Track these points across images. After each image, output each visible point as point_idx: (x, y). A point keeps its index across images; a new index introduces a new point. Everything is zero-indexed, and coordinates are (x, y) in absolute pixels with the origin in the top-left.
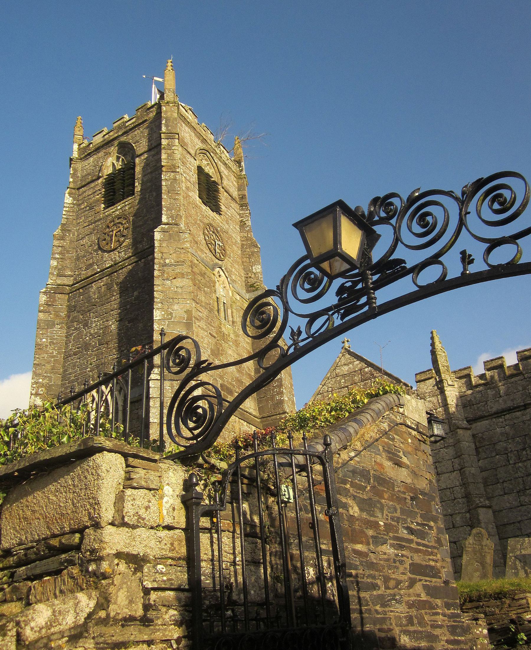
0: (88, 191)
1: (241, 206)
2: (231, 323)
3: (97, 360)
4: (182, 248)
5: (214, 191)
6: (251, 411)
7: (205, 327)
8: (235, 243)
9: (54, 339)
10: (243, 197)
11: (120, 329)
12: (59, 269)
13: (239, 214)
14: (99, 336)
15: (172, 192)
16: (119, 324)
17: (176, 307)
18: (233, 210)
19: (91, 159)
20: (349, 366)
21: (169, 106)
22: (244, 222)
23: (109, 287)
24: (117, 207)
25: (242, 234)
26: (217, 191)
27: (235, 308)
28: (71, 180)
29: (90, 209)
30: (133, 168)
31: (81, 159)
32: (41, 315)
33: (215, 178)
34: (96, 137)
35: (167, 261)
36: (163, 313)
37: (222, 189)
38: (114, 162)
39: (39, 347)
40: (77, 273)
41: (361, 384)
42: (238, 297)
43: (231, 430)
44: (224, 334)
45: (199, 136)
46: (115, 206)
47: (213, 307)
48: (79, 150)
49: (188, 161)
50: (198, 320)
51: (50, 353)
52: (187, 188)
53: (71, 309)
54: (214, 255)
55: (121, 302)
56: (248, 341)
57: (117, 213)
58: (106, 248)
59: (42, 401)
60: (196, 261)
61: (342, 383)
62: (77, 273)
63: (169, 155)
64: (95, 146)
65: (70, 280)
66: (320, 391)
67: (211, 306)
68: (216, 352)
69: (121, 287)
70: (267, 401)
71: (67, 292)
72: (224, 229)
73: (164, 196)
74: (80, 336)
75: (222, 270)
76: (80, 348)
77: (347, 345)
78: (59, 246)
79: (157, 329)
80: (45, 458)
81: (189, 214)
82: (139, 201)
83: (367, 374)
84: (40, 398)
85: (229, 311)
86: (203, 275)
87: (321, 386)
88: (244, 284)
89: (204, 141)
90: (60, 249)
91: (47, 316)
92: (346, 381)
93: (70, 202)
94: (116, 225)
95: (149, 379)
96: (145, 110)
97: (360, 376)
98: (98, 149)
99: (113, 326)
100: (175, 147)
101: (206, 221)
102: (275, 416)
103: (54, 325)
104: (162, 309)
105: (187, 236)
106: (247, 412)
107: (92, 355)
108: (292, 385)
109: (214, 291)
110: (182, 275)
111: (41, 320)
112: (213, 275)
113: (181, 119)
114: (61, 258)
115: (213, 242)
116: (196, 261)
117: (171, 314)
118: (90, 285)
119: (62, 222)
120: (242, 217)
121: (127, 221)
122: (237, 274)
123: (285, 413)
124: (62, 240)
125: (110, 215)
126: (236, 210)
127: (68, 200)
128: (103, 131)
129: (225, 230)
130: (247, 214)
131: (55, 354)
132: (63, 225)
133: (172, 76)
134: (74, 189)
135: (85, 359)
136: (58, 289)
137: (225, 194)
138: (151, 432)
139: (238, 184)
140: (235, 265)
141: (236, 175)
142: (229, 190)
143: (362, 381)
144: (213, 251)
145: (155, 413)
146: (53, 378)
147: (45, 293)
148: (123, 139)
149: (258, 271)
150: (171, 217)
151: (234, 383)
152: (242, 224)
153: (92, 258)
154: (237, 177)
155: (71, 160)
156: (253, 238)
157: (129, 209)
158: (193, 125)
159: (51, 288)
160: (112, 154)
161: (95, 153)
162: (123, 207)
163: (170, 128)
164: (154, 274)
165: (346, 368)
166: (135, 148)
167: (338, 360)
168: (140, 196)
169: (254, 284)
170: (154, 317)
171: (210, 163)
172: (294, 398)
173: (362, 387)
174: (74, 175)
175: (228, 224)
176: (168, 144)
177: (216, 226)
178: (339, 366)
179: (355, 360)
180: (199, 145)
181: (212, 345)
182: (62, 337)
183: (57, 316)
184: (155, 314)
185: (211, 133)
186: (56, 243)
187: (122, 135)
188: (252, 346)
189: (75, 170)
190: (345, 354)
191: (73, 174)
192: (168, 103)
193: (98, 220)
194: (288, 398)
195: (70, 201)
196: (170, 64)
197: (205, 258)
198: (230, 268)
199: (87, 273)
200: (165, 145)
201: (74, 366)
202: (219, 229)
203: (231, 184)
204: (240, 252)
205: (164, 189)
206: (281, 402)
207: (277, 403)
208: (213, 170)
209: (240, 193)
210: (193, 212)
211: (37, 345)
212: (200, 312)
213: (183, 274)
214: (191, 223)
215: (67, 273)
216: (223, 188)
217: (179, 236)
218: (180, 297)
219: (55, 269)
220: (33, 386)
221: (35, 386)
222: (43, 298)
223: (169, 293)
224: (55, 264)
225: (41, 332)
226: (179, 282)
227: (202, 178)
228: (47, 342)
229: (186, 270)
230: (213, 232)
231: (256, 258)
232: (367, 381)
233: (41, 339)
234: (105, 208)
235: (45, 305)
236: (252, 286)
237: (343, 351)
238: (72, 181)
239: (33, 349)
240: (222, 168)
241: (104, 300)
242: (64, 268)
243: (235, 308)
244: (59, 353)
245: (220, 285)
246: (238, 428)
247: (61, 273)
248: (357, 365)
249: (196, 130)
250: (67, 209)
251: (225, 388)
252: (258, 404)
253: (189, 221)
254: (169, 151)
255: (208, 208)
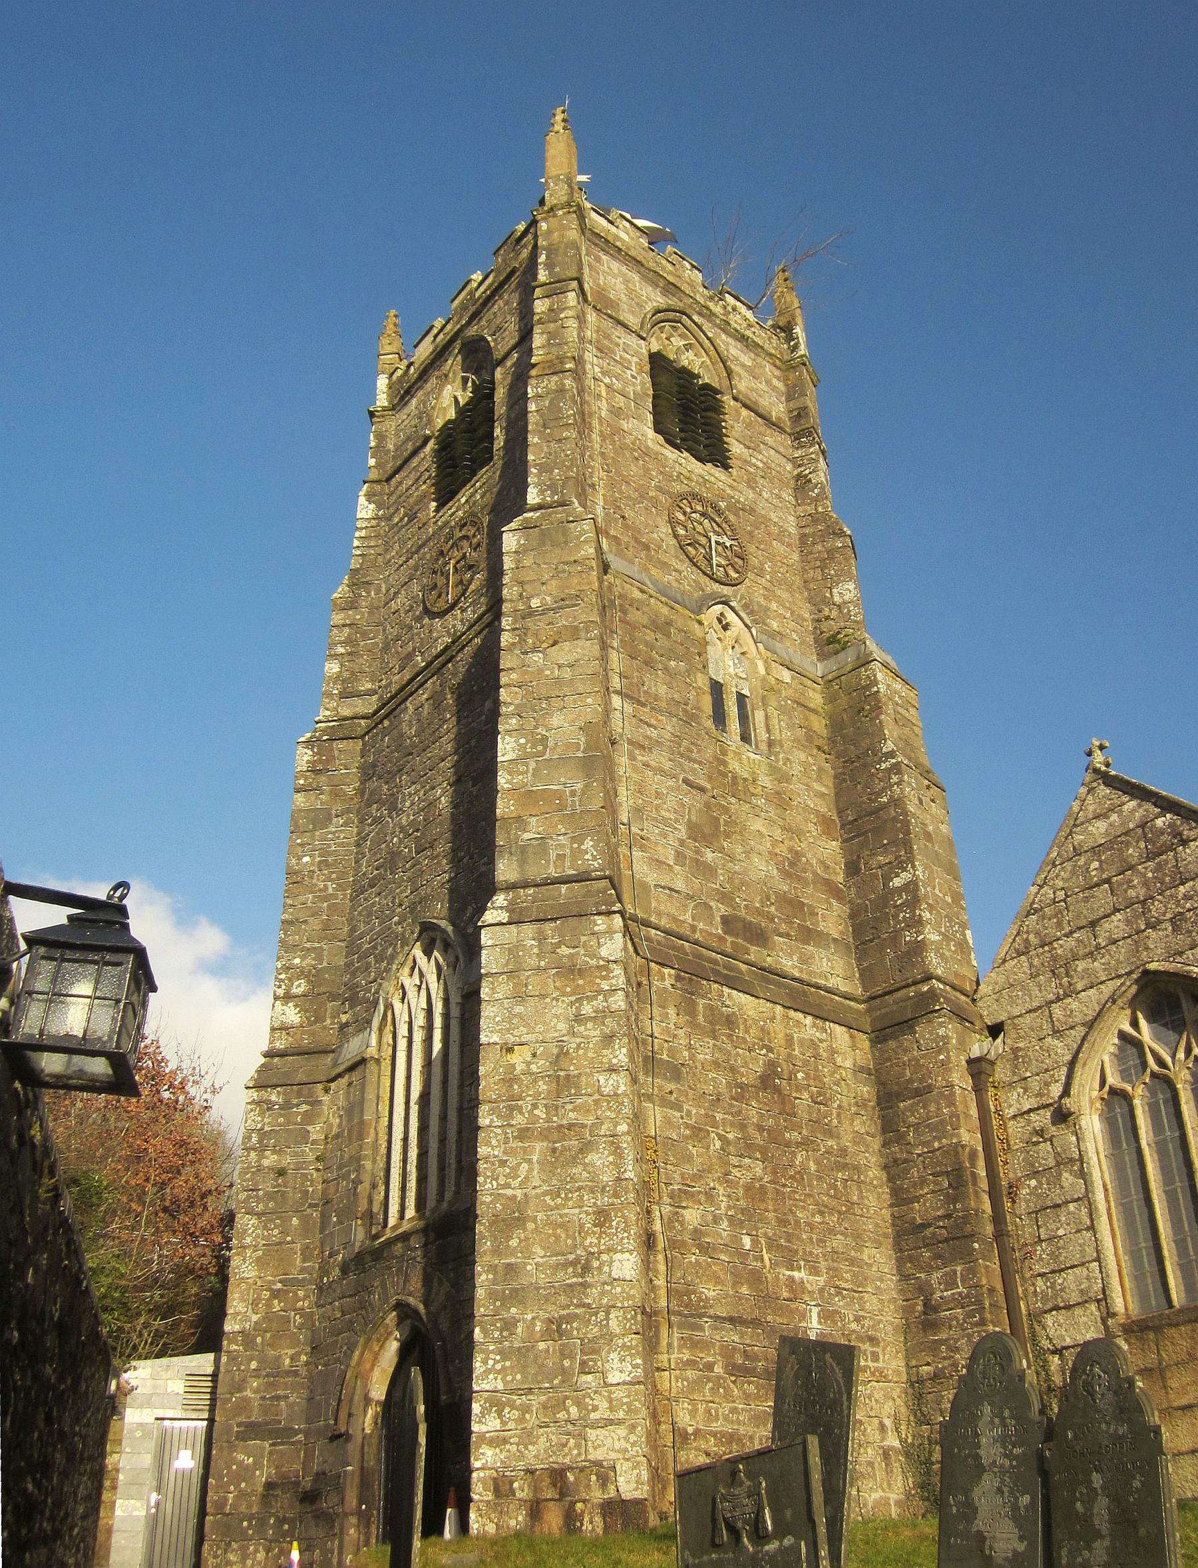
0: (405, 479)
1: (796, 439)
2: (763, 747)
3: (412, 893)
4: (575, 561)
5: (706, 410)
6: (832, 983)
7: (667, 765)
8: (782, 534)
9: (329, 854)
10: (800, 414)
11: (455, 805)
12: (343, 681)
13: (793, 460)
14: (417, 830)
15: (552, 424)
16: (454, 791)
17: (556, 720)
18: (772, 452)
19: (414, 402)
20: (1108, 818)
21: (555, 216)
22: (806, 476)
23: (437, 700)
24: (459, 500)
25: (800, 509)
26: (716, 408)
27: (775, 704)
28: (372, 462)
29: (410, 521)
30: (491, 396)
31: (393, 409)
32: (300, 799)
33: (708, 376)
34: (420, 345)
35: (535, 603)
36: (523, 741)
37: (732, 403)
38: (456, 394)
39: (295, 879)
40: (384, 682)
41: (1146, 868)
42: (786, 676)
43: (754, 1044)
44: (735, 778)
45: (654, 278)
46: (455, 500)
47: (698, 709)
48: (390, 388)
49: (618, 345)
50: (643, 747)
51: (320, 890)
52: (616, 412)
53: (368, 772)
54: (705, 573)
55: (459, 733)
56: (823, 789)
57: (460, 513)
58: (441, 605)
59: (299, 1012)
60: (637, 594)
61: (1093, 873)
62: (384, 682)
63: (551, 335)
64: (419, 368)
65: (370, 704)
66: (1033, 902)
67: (689, 708)
68: (706, 830)
69: (459, 696)
70: (881, 950)
71: (360, 731)
72: (739, 502)
73: (533, 439)
74: (381, 839)
75: (732, 609)
76: (381, 867)
77: (1098, 758)
78: (344, 625)
79: (506, 786)
80: (1049, 1117)
81: (621, 475)
82: (501, 472)
83: (1162, 833)
84: (296, 1006)
85: (759, 716)
86: (661, 627)
87: (1034, 889)
88: (810, 640)
89: (670, 288)
90: (347, 630)
91: (313, 798)
92: (1105, 866)
93: (370, 515)
94: (457, 546)
95: (480, 924)
96: (512, 247)
97: (1142, 845)
98: (424, 375)
99: (443, 798)
100: (566, 312)
101: (677, 488)
102: (904, 991)
103: (329, 819)
104: (519, 730)
105: (586, 527)
106: (819, 988)
107: (403, 881)
108: (957, 898)
109: (700, 667)
110: (574, 633)
111: (300, 811)
112: (697, 626)
113: (596, 245)
114: (350, 654)
115: (703, 541)
116: (637, 594)
117: (544, 739)
118: (403, 706)
119: (352, 567)
120: (799, 466)
121: (478, 529)
122: (788, 615)
123: (928, 978)
124: (350, 609)
125: (446, 523)
126: (781, 450)
127: (365, 510)
128: (433, 326)
129: (744, 504)
130: (813, 456)
131: (330, 891)
132: (354, 572)
133: (562, 145)
134: (378, 482)
135: (390, 893)
136: (341, 731)
137: (745, 413)
138: (482, 1070)
139: (786, 385)
140: (778, 593)
141: (778, 362)
142: (755, 403)
143: (1148, 859)
144: (703, 564)
145: (495, 1016)
146: (325, 953)
147: (309, 743)
148: (472, 331)
149: (847, 597)
150: (549, 487)
151: (773, 908)
152: (802, 484)
153: (412, 639)
154: (783, 367)
155: (372, 414)
156: (832, 514)
157: (482, 497)
158: (632, 253)
159: (324, 731)
160: (451, 375)
161: (419, 384)
162: (470, 497)
163: (557, 269)
164: (500, 642)
165: (1101, 826)
166: (492, 344)
167: (1076, 806)
168: (503, 458)
169: (839, 633)
170: (499, 754)
171: (693, 341)
172: (968, 933)
173: (1150, 875)
174: (379, 450)
175: (753, 489)
176: (551, 310)
177: (715, 499)
178: (1082, 823)
179: (1125, 798)
180: (658, 299)
181: (693, 812)
182: (348, 844)
183: (336, 794)
184: (500, 746)
185: (693, 266)
186: (338, 618)
187: (469, 323)
188: (837, 801)
189: (381, 437)
190: (1095, 784)
191: (377, 447)
192: (552, 209)
193: (424, 545)
194: (941, 933)
195: (370, 512)
196: (559, 117)
197: (675, 584)
198: (763, 603)
199: (402, 679)
200: (543, 312)
201: (370, 915)
202: (722, 505)
203: (763, 386)
204: (796, 557)
205: (533, 419)
206: (918, 948)
207: (908, 953)
208: (705, 358)
209: (792, 405)
210: (634, 470)
211: (290, 873)
212: (649, 725)
213: (576, 629)
214: (629, 498)
215: (363, 685)
216: (735, 399)
217: (565, 532)
218: (567, 691)
219: (335, 683)
220: (280, 977)
221: (283, 976)
222: (304, 757)
223: (537, 685)
224: (334, 671)
225: (299, 841)
226: (566, 653)
227: (663, 379)
228: (312, 864)
229: (583, 618)
230: (703, 514)
231: (840, 564)
232: (1164, 857)
233: (300, 858)
234: (437, 510)
235: (308, 774)
236: (832, 640)
237: (1088, 777)
238: (373, 464)
239: (281, 881)
240: (733, 349)
241: (428, 737)
242: (354, 676)
243: (775, 704)
244: (340, 887)
245: (725, 649)
246: (781, 1035)
247: (348, 690)
248: (1133, 811)
249: (642, 265)
250: (363, 533)
251: (740, 925)
252: (859, 960)
253: (621, 492)
254: (552, 325)
255: (686, 454)
